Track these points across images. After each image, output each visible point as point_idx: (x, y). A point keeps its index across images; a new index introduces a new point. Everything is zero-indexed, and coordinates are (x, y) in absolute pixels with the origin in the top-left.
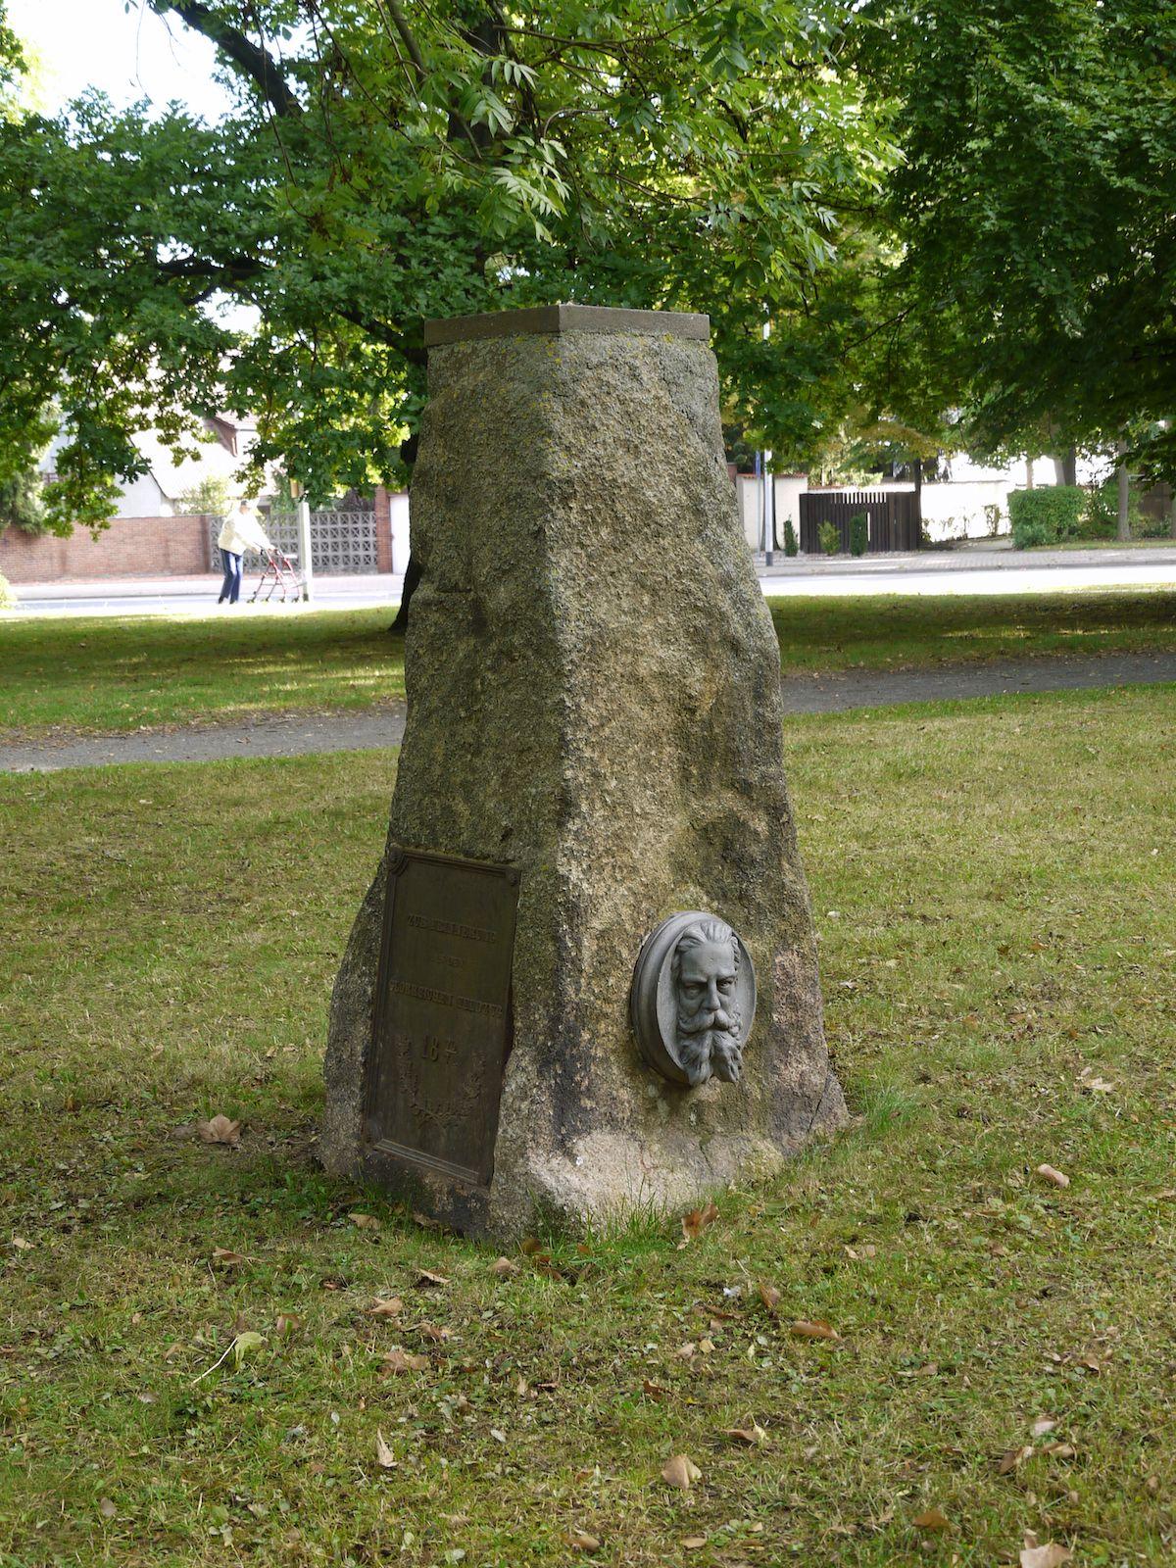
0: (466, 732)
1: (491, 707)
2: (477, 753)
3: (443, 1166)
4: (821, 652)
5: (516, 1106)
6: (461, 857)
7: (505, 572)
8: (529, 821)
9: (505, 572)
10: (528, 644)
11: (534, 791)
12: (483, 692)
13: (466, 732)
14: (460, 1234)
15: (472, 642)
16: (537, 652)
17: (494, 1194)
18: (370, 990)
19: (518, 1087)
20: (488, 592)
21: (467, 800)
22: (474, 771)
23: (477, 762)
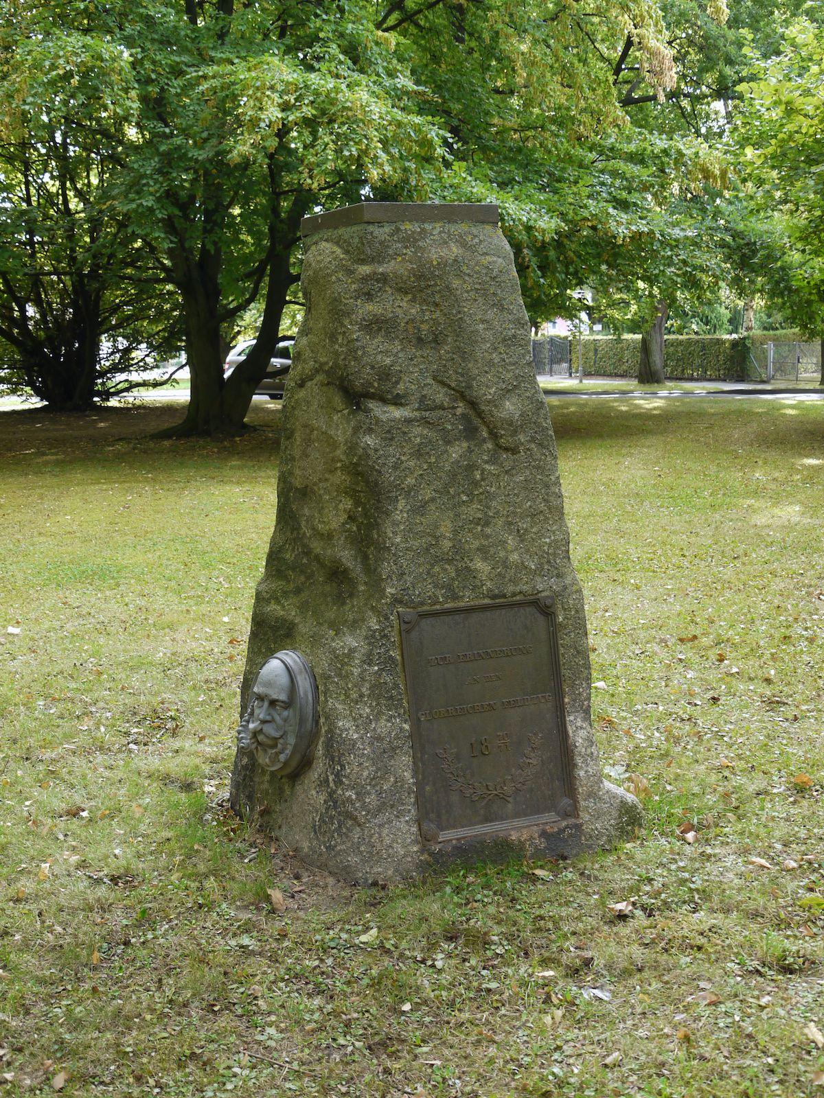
0: (473, 510)
1: (493, 489)
2: (487, 524)
3: (517, 822)
4: (102, 490)
5: (589, 751)
6: (487, 601)
7: (508, 391)
8: (549, 562)
9: (508, 391)
10: (533, 440)
11: (548, 540)
12: (483, 479)
13: (473, 510)
14: (564, 858)
15: (465, 445)
16: (541, 445)
17: (584, 816)
18: (406, 727)
19: (585, 740)
20: (496, 406)
21: (485, 559)
22: (487, 537)
23: (488, 530)
